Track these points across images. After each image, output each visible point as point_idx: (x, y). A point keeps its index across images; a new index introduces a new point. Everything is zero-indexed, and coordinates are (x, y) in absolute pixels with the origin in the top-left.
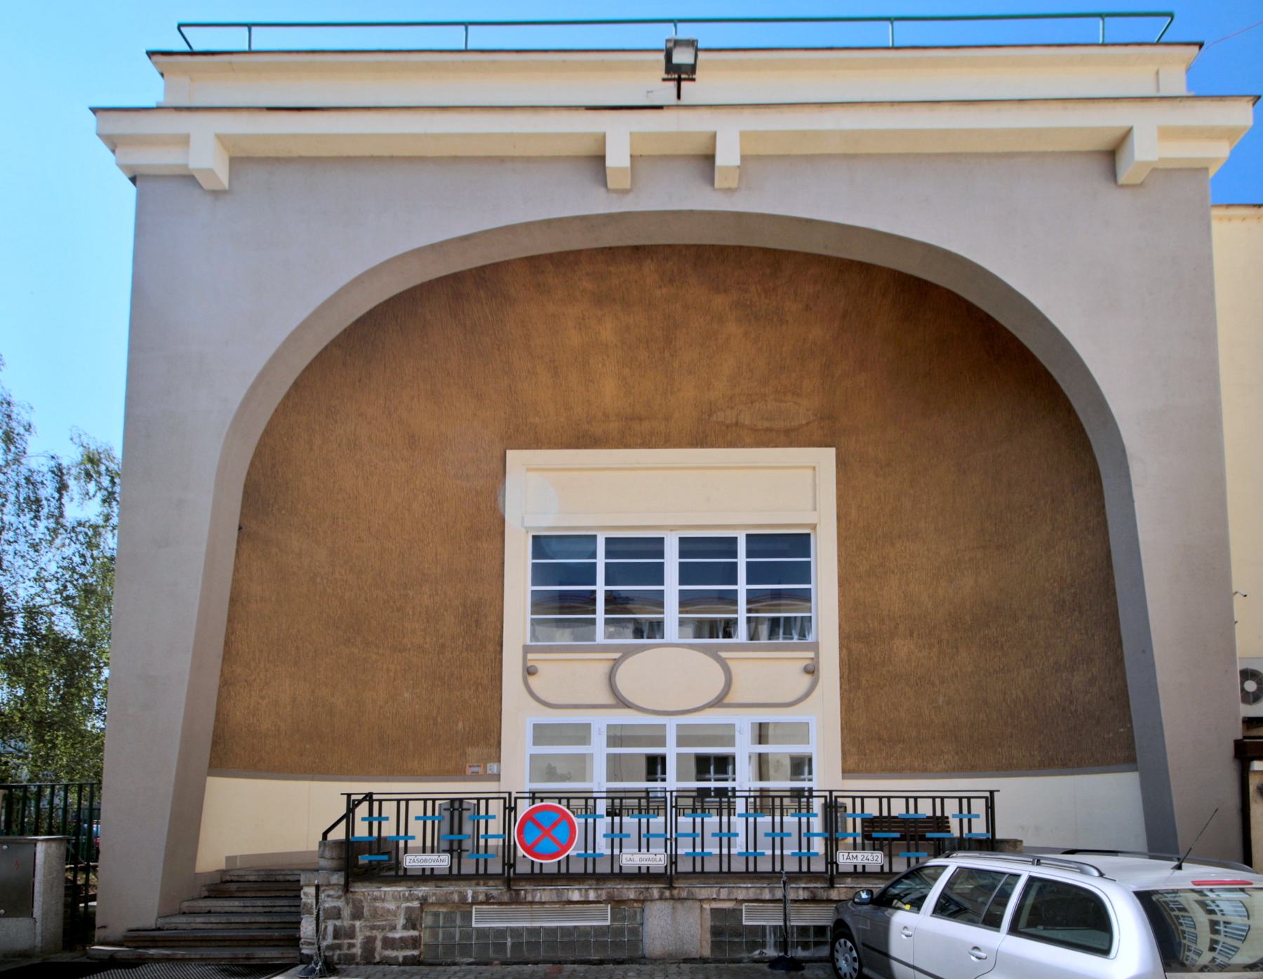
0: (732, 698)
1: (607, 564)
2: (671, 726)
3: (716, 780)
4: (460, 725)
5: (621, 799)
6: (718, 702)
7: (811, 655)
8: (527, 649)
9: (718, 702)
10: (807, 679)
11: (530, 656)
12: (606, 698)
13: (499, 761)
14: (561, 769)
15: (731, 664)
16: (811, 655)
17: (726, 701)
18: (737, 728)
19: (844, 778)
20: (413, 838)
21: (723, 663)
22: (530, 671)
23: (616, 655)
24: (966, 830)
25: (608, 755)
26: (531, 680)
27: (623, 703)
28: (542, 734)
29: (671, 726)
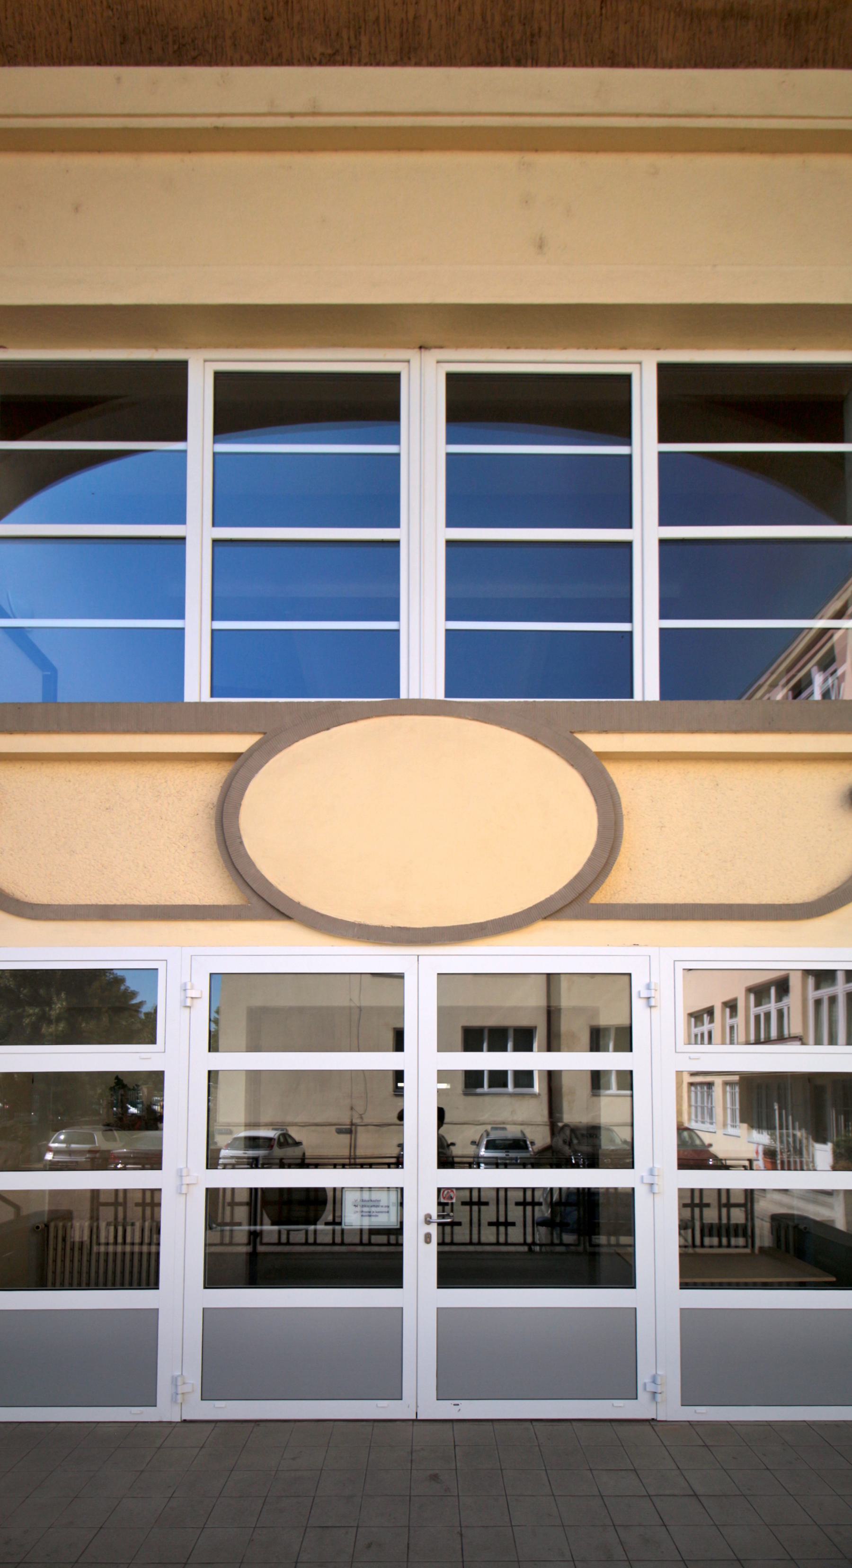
0: (617, 889)
1: (663, 457)
2: (422, 976)
3: (496, 1164)
5: (720, 1245)
6: (576, 901)
9: (576, 901)
12: (210, 886)
14: (310, 1141)
15: (618, 773)
17: (600, 897)
18: (638, 986)
21: (594, 772)
23: (240, 743)
27: (263, 902)
29: (422, 976)
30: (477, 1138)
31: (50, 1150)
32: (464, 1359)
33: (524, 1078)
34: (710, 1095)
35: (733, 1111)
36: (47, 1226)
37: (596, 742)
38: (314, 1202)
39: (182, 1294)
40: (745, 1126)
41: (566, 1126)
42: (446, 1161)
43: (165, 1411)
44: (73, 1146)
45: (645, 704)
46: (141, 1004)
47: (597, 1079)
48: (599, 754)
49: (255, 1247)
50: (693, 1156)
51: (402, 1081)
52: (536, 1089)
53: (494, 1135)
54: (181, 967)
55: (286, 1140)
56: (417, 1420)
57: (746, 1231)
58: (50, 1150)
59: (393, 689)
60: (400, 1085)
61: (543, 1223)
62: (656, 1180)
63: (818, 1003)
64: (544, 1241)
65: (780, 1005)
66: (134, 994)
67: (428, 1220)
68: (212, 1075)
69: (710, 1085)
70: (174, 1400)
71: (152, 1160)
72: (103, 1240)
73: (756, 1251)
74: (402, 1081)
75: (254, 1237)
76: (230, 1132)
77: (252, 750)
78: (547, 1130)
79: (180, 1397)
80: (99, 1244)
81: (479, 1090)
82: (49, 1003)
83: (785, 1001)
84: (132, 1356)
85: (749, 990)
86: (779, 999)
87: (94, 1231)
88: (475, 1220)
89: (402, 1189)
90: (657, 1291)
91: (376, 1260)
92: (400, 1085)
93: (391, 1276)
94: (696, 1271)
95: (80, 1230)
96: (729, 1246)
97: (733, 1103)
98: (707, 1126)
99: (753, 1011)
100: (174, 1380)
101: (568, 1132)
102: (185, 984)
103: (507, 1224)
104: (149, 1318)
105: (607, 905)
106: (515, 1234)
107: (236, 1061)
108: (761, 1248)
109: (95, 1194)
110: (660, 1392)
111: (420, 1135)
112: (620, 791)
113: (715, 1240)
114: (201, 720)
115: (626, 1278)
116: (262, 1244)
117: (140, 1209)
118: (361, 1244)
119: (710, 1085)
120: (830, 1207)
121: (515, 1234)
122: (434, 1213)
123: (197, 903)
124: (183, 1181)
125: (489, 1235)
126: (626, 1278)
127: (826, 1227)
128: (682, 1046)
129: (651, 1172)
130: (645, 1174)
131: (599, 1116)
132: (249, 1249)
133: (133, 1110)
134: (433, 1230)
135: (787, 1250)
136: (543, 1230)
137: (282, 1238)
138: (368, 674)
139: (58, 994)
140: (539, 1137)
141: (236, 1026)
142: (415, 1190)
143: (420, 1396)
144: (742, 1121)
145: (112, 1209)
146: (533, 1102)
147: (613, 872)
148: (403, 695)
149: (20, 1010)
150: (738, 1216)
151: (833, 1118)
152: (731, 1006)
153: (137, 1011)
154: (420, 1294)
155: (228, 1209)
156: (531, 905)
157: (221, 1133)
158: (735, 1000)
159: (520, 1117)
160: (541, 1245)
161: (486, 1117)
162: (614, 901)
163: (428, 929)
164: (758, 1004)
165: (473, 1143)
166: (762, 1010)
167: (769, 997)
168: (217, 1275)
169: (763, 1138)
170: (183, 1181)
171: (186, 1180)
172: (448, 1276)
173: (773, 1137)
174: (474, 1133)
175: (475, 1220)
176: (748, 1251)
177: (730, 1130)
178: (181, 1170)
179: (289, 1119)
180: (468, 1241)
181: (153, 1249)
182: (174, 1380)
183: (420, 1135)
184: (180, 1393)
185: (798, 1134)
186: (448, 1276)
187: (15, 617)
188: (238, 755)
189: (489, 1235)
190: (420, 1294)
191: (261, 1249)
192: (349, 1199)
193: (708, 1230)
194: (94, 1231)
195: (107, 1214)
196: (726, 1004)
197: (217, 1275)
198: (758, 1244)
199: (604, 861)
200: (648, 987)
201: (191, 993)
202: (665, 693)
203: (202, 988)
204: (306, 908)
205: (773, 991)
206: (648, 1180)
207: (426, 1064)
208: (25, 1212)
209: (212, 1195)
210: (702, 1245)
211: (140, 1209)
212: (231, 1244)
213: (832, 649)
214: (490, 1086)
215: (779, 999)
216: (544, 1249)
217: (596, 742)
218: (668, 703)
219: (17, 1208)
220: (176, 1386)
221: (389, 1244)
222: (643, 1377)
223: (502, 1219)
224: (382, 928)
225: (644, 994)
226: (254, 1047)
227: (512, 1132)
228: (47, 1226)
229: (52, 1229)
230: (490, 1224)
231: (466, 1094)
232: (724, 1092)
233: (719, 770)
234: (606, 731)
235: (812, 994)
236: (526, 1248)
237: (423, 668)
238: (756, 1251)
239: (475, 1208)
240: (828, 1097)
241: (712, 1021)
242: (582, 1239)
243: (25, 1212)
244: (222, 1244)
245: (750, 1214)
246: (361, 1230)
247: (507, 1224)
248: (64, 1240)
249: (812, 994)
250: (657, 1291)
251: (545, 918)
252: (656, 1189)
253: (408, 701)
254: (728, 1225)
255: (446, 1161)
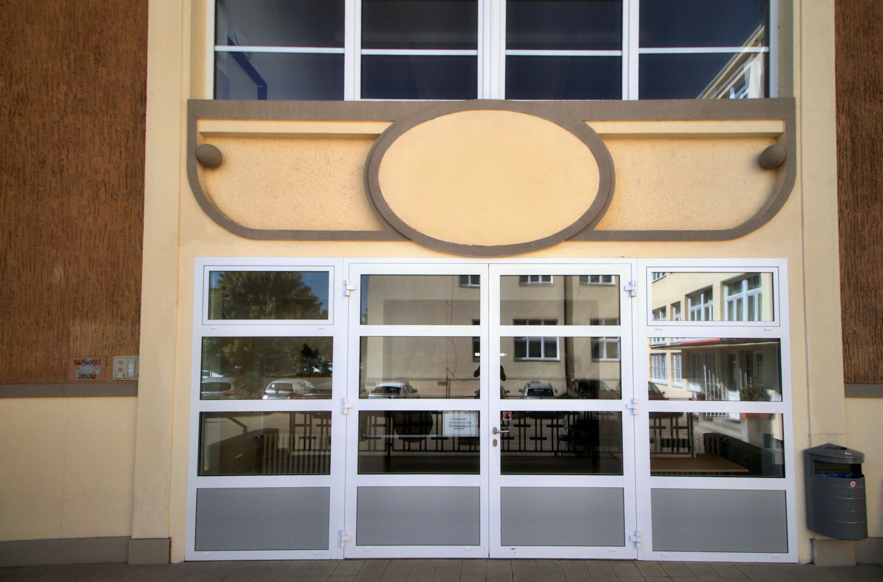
0: (613, 220)
2: (492, 273)
4: (58, 272)
5: (672, 453)
6: (586, 229)
7: (776, 126)
8: (196, 110)
9: (586, 229)
10: (760, 186)
11: (205, 126)
13: (441, 413)
15: (615, 149)
16: (776, 126)
17: (601, 227)
18: (624, 283)
19: (848, 394)
20: (548, 426)
21: (598, 147)
22: (205, 159)
23: (378, 128)
24: (539, 431)
25: (654, 491)
26: (217, 184)
27: (392, 229)
28: (240, 293)
30: (522, 388)
31: (266, 394)
32: (518, 518)
33: (551, 345)
34: (663, 360)
35: (678, 370)
36: (262, 437)
37: (599, 127)
38: (424, 422)
39: (344, 478)
40: (685, 381)
41: (577, 380)
42: (504, 395)
43: (334, 552)
44: (280, 392)
45: (629, 102)
46: (321, 304)
47: (596, 346)
48: (600, 135)
49: (389, 453)
50: (655, 394)
51: (479, 351)
52: (558, 358)
53: (533, 386)
54: (344, 269)
55: (408, 389)
56: (489, 559)
57: (688, 443)
58: (266, 394)
59: (475, 96)
60: (477, 354)
61: (564, 438)
62: (635, 406)
63: (730, 303)
64: (564, 449)
65: (707, 305)
66: (316, 298)
67: (495, 431)
68: (363, 340)
69: (664, 355)
70: (339, 545)
71: (327, 394)
72: (296, 448)
73: (695, 456)
74: (479, 351)
75: (389, 444)
76: (375, 384)
77: (387, 132)
78: (565, 383)
79: (343, 544)
80: (294, 450)
81: (523, 358)
82: (265, 303)
83: (710, 302)
84: (314, 515)
85: (688, 296)
86: (706, 301)
87: (292, 442)
88: (522, 439)
89: (479, 412)
90: (637, 476)
91: (463, 457)
92: (477, 354)
93: (471, 465)
94: (660, 465)
95: (283, 442)
96: (678, 453)
97: (678, 366)
98: (661, 381)
99: (690, 308)
100: (340, 532)
101: (577, 385)
102: (343, 399)
103: (542, 439)
104: (324, 493)
105: (604, 231)
106: (547, 445)
107: (378, 330)
108: (697, 455)
109: (292, 414)
110: (639, 543)
111: (490, 380)
112: (614, 159)
113: (670, 449)
114: (355, 113)
115: (616, 468)
116: (393, 450)
117: (320, 428)
118: (454, 451)
119: (664, 355)
120: (739, 431)
121: (547, 445)
122: (499, 428)
123: (353, 229)
124: (346, 405)
125: (531, 445)
126: (616, 468)
127: (739, 442)
128: (652, 322)
129: (632, 402)
130: (629, 403)
131: (598, 374)
132: (386, 453)
133: (316, 370)
134: (498, 437)
135: (716, 453)
136: (562, 443)
137: (407, 442)
138: (456, 83)
139: (271, 299)
140: (560, 386)
141: (376, 309)
142: (485, 410)
143: (491, 544)
144: (683, 377)
145: (302, 428)
146: (556, 365)
147: (608, 211)
148: (480, 97)
149: (247, 308)
150: (683, 435)
151: (738, 373)
152: (676, 305)
153: (318, 309)
154: (490, 480)
155: (373, 428)
156: (558, 231)
157: (369, 384)
158: (679, 303)
159: (548, 375)
160: (562, 452)
161: (527, 375)
162: (609, 229)
163: (495, 247)
164: (693, 304)
165: (520, 391)
166: (696, 308)
167: (700, 300)
168: (366, 466)
169: (697, 388)
170: (346, 405)
171: (347, 406)
172: (509, 466)
173: (703, 387)
174: (521, 384)
175: (522, 439)
176: (689, 456)
177: (676, 383)
178: (343, 399)
179: (409, 375)
180: (518, 448)
181: (327, 453)
182: (340, 532)
183: (490, 380)
184: (343, 542)
185: (718, 385)
186: (509, 466)
187: (238, 45)
188: (378, 135)
189: (531, 445)
190: (490, 480)
191: (392, 454)
192: (447, 419)
193: (665, 443)
194: (292, 442)
195: (299, 432)
196: (673, 305)
197: (366, 466)
198: (696, 451)
199: (603, 203)
200: (630, 284)
201: (349, 287)
202: (641, 96)
203: (355, 284)
204: (419, 233)
205: (702, 296)
206: (630, 406)
207: (493, 332)
208: (249, 430)
209: (364, 416)
210: (661, 453)
211: (320, 428)
212: (375, 450)
213: (743, 76)
214: (530, 356)
215: (706, 301)
216: (564, 454)
217: (599, 127)
218: (644, 101)
219: (245, 427)
220: (341, 536)
221: (470, 451)
222: (629, 532)
223: (539, 435)
224: (466, 246)
225: (628, 288)
226: (388, 321)
227: (544, 384)
228: (262, 437)
229: (265, 439)
230: (532, 438)
231: (516, 361)
232: (672, 359)
233: (676, 145)
234: (605, 120)
235: (727, 298)
236: (553, 454)
237: (492, 79)
238: (695, 456)
239: (522, 429)
240: (736, 362)
241: (664, 316)
242: (588, 445)
243: (249, 430)
244: (369, 450)
245: (691, 433)
246: (454, 438)
247: (542, 439)
248: (273, 446)
249: (727, 298)
250: (637, 476)
251: (567, 240)
252: (635, 412)
253: (483, 100)
254: (678, 440)
255: (504, 395)
